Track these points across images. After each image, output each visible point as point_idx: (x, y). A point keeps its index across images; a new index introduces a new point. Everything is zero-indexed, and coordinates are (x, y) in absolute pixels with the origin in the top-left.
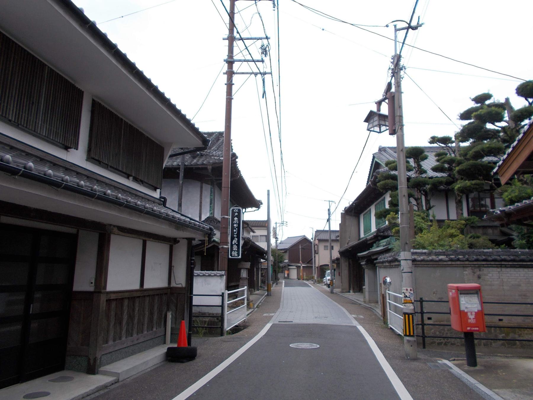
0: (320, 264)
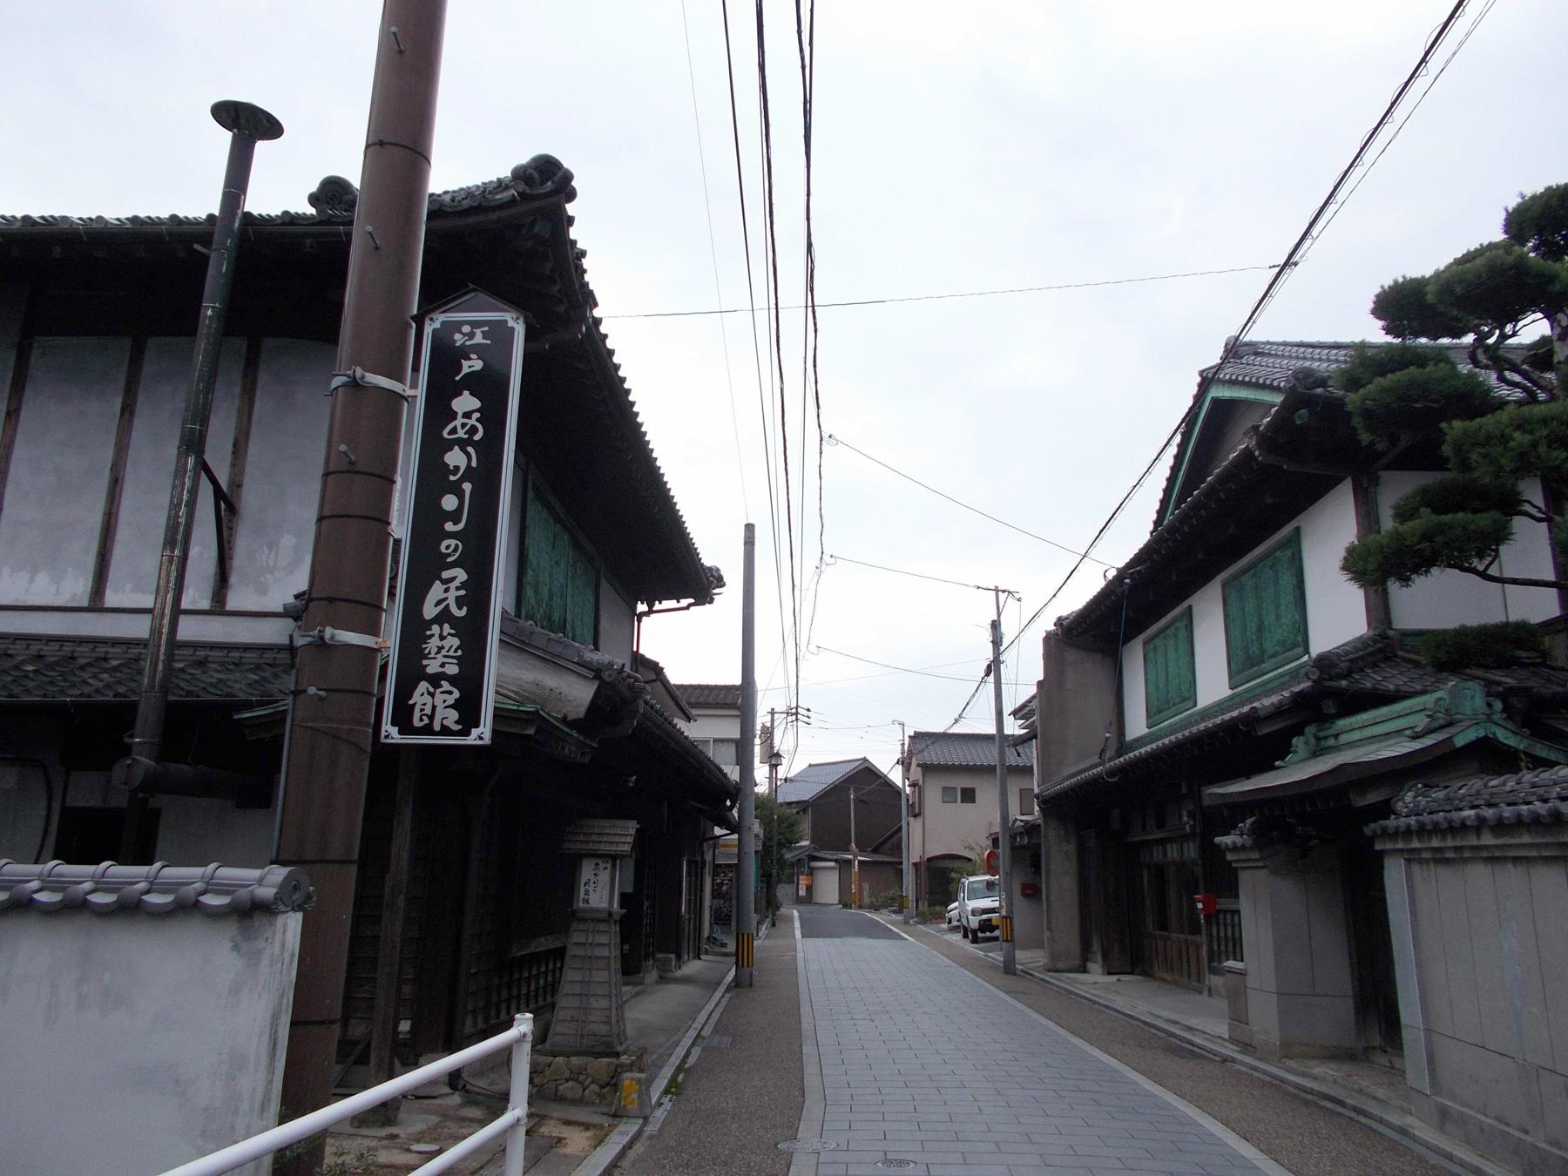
0: (929, 855)
